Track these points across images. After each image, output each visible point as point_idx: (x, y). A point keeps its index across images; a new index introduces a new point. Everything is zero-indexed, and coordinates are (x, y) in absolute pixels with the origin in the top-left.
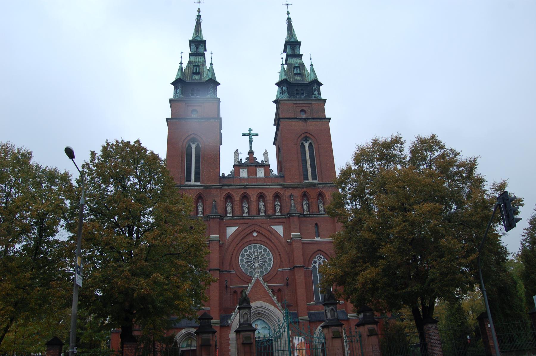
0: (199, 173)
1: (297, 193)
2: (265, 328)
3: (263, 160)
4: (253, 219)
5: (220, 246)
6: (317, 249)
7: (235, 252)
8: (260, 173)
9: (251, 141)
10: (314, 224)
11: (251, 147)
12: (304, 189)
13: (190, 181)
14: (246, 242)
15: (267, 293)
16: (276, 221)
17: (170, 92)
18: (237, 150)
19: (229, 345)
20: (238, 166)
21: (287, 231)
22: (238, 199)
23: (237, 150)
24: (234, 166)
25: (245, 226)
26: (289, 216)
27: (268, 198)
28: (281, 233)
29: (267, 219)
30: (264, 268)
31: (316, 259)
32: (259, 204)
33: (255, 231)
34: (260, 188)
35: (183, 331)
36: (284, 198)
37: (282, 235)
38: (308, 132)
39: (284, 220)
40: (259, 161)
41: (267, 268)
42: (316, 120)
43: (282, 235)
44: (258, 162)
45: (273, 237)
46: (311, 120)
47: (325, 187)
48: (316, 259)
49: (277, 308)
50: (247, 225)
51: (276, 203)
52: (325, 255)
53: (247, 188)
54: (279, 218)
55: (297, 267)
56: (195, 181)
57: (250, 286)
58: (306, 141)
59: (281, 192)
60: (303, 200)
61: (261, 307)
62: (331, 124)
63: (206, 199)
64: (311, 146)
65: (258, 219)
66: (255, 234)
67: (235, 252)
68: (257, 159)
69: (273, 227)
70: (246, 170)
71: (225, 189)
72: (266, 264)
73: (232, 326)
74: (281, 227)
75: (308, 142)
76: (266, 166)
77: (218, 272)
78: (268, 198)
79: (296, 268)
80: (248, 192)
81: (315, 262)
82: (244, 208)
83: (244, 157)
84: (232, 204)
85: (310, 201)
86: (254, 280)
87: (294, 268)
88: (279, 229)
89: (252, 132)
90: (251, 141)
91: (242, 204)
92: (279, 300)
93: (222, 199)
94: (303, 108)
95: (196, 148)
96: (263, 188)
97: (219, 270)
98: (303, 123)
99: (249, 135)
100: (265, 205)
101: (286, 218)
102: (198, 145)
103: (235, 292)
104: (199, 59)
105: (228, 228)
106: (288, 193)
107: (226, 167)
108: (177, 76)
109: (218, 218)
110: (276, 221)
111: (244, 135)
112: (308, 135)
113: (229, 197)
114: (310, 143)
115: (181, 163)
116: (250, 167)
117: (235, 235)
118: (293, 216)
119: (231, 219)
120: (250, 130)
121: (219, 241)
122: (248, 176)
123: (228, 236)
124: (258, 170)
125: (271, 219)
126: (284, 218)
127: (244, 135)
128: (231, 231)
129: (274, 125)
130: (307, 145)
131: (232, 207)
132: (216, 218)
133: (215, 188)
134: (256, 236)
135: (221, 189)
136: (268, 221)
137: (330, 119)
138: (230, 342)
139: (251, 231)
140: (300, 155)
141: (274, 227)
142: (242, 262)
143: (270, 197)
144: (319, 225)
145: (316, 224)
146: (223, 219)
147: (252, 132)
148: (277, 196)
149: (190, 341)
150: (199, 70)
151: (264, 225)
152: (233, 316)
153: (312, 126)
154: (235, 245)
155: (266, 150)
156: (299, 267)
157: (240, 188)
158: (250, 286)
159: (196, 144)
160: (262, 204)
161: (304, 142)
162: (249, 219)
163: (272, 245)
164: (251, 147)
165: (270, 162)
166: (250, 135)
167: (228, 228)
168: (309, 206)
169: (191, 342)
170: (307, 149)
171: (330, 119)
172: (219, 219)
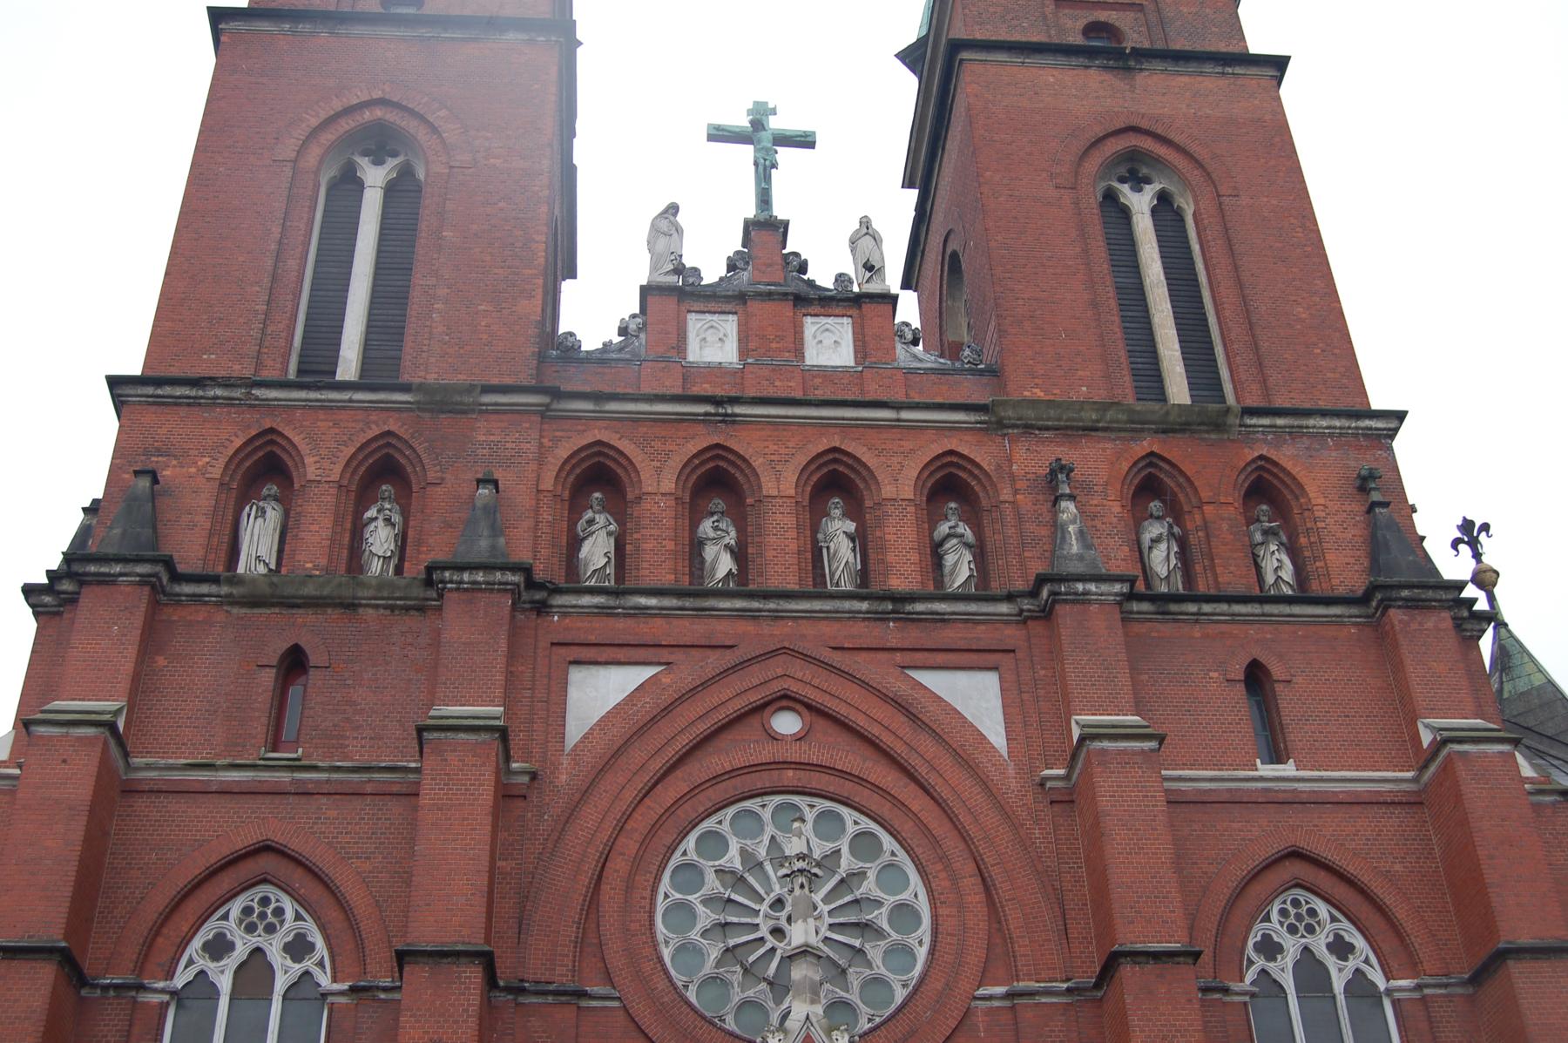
0: (399, 334)
1: (1101, 463)
3: (850, 270)
4: (777, 616)
5: (506, 795)
7: (628, 844)
9: (764, 171)
10: (1238, 670)
11: (764, 199)
14: (716, 779)
16: (948, 636)
18: (673, 209)
20: (672, 295)
22: (668, 484)
23: (673, 209)
24: (645, 291)
25: (715, 662)
26: (1045, 598)
27: (888, 491)
28: (995, 732)
29: (882, 617)
30: (856, 976)
31: (1275, 927)
33: (786, 701)
34: (825, 425)
36: (1006, 494)
37: (996, 735)
38: (1144, 124)
39: (1012, 635)
40: (822, 275)
41: (878, 981)
42: (1192, 67)
43: (996, 735)
44: (811, 283)
46: (1159, 65)
47: (1295, 434)
48: (1275, 927)
50: (730, 658)
54: (970, 620)
58: (1138, 182)
59: (983, 453)
60: (1139, 518)
62: (1290, 91)
63: (432, 475)
65: (810, 616)
66: (787, 723)
68: (803, 268)
69: (933, 680)
70: (729, 325)
71: (575, 418)
72: (875, 952)
75: (1150, 191)
77: (473, 975)
78: (888, 491)
79: (1127, 970)
80: (740, 442)
82: (710, 552)
83: (710, 252)
84: (621, 522)
85: (1194, 521)
87: (1112, 963)
88: (975, 698)
89: (775, 123)
90: (764, 171)
91: (694, 524)
93: (548, 483)
94: (1102, 16)
95: (390, 190)
96: (847, 427)
97: (487, 960)
98: (1108, 77)
100: (860, 539)
101: (1023, 619)
102: (406, 172)
105: (577, 675)
106: (1030, 458)
107: (596, 307)
109: (504, 588)
110: (948, 636)
111: (719, 135)
112: (1147, 144)
113: (599, 477)
114: (1163, 198)
115: (278, 259)
116: (754, 306)
117: (631, 725)
118: (1083, 599)
119: (603, 612)
121: (503, 733)
122: (743, 352)
123: (576, 726)
125: (904, 616)
126: (1004, 620)
127: (719, 135)
128: (598, 693)
129: (908, 183)
130: (1140, 203)
132: (490, 587)
133: (498, 410)
134: (799, 738)
135: (544, 414)
136: (892, 633)
137: (1279, 64)
139: (755, 698)
140: (1102, 266)
142: (682, 929)
143: (897, 479)
144: (1276, 670)
145: (1256, 678)
146: (542, 608)
147: (775, 123)
148: (949, 485)
153: (1161, 97)
154: (630, 795)
155: (865, 223)
156: (1156, 956)
157: (682, 419)
159: (391, 163)
160: (838, 530)
161: (1125, 188)
162: (742, 614)
163: (918, 802)
164: (764, 199)
166: (764, 139)
168: (1184, 554)
170: (1144, 225)
171: (1279, 64)
172: (515, 591)
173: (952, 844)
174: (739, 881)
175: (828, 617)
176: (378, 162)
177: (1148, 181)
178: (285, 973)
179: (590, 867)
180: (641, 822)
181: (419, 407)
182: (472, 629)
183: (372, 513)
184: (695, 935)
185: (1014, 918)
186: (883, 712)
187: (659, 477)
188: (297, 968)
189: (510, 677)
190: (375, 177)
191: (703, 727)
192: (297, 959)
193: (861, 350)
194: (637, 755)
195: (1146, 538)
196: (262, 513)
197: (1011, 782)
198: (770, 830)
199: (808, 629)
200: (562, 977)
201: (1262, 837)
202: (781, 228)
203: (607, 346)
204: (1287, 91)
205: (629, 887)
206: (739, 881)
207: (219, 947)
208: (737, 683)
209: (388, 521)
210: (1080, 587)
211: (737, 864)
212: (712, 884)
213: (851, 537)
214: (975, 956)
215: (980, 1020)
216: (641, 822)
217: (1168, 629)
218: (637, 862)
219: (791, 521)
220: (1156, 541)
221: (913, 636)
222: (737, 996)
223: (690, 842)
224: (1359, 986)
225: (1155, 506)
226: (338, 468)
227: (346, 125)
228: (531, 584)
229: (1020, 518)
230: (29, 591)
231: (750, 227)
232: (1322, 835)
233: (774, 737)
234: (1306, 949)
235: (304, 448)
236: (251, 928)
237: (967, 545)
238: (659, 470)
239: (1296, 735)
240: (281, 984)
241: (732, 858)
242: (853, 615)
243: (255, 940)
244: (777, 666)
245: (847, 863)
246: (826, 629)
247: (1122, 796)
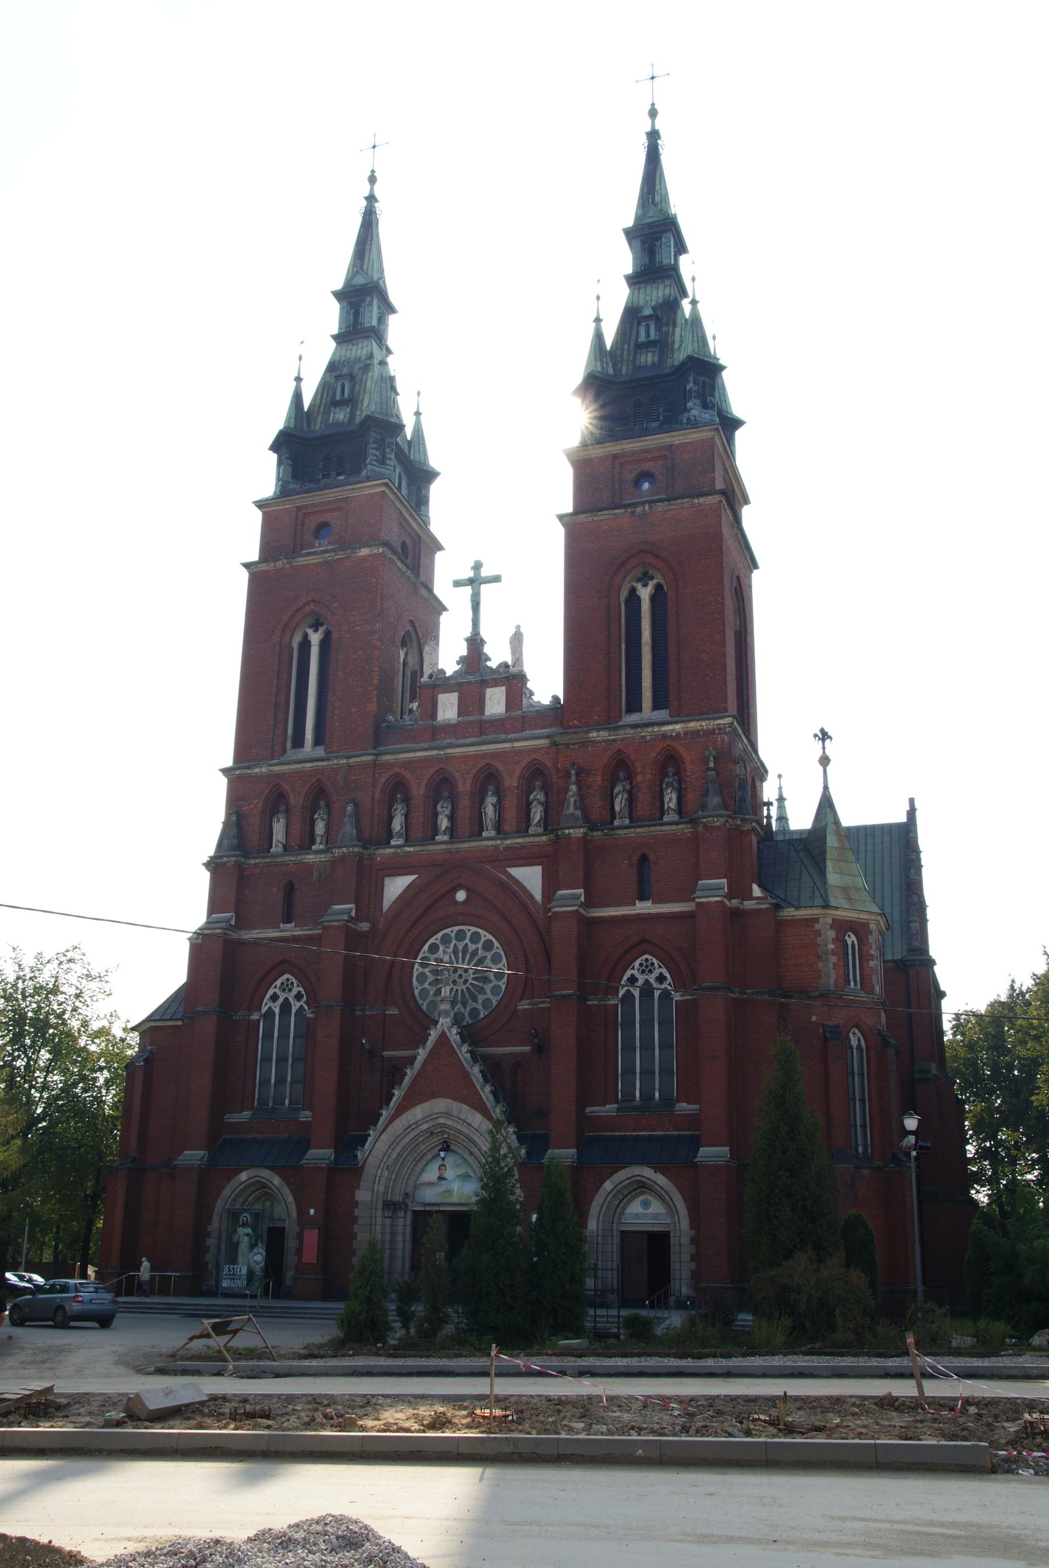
8: (495, 702)
13: (639, 709)
15: (466, 1077)
17: (264, 476)
19: (354, 1220)
21: (550, 885)
22: (422, 791)
32: (391, 806)
51: (532, 797)
56: (656, 707)
57: (422, 1054)
61: (448, 1114)
64: (325, 644)
73: (367, 1166)
74: (538, 869)
76: (513, 680)
78: (507, 783)
82: (440, 817)
84: (408, 806)
86: (434, 1034)
89: (485, 573)
91: (529, 793)
95: (653, 598)
99: (471, 582)
104: (658, 293)
108: (587, 366)
114: (658, 587)
120: (477, 566)
122: (459, 714)
123: (387, 904)
124: (489, 692)
131: (406, 816)
134: (465, 902)
138: (357, 1212)
141: (516, 872)
144: (652, 857)
147: (485, 573)
149: (268, 1204)
150: (352, 389)
152: (370, 1139)
155: (518, 627)
158: (422, 1054)
159: (321, 630)
160: (491, 800)
165: (529, 668)
167: (387, 881)
174: (464, 952)
177: (652, 578)
178: (295, 1006)
183: (316, 816)
184: (426, 985)
188: (298, 1004)
192: (299, 1001)
195: (615, 791)
196: (278, 821)
198: (454, 942)
202: (482, 642)
207: (274, 998)
209: (322, 819)
210: (567, 831)
211: (470, 950)
213: (494, 806)
220: (619, 793)
224: (665, 995)
226: (301, 799)
230: (204, 864)
234: (647, 980)
235: (289, 791)
236: (643, 972)
237: (541, 803)
238: (419, 784)
240: (657, 993)
243: (285, 995)
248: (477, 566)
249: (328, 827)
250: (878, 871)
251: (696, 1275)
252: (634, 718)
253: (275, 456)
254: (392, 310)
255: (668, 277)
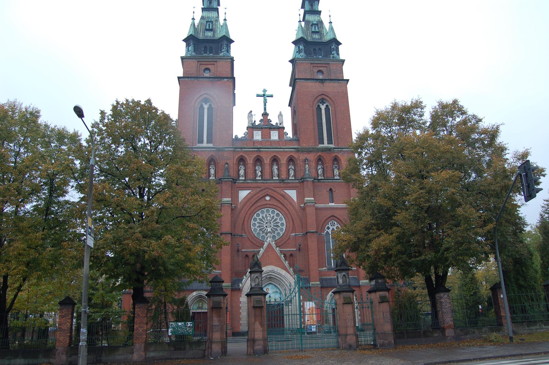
2: (276, 292)
3: (278, 122)
4: (266, 183)
5: (232, 210)
6: (330, 215)
7: (248, 216)
8: (274, 136)
10: (328, 189)
11: (265, 109)
12: (319, 154)
16: (290, 185)
18: (251, 112)
19: (240, 308)
20: (252, 127)
21: (301, 196)
22: (251, 162)
23: (251, 112)
24: (248, 128)
27: (282, 162)
29: (281, 183)
30: (276, 232)
32: (272, 167)
33: (268, 195)
34: (273, 152)
35: (194, 293)
36: (299, 162)
37: (295, 200)
39: (298, 185)
40: (274, 123)
42: (333, 81)
43: (295, 200)
45: (286, 201)
46: (328, 81)
47: (341, 151)
49: (289, 272)
52: (338, 221)
53: (260, 151)
54: (293, 183)
55: (309, 232)
57: (262, 251)
58: (323, 103)
59: (296, 156)
60: (317, 164)
61: (273, 271)
64: (327, 108)
65: (271, 183)
66: (268, 198)
67: (248, 216)
72: (278, 229)
75: (325, 105)
77: (230, 236)
78: (282, 162)
79: (308, 234)
81: (328, 228)
82: (257, 172)
83: (258, 119)
87: (307, 233)
88: (293, 194)
91: (255, 167)
92: (291, 265)
95: (208, 109)
96: (276, 152)
97: (231, 234)
100: (278, 169)
101: (300, 183)
102: (210, 105)
103: (247, 256)
105: (240, 192)
106: (302, 157)
110: (290, 185)
111: (258, 96)
112: (325, 97)
114: (327, 106)
116: (264, 130)
117: (248, 199)
118: (307, 181)
120: (265, 91)
122: (262, 138)
123: (240, 200)
125: (284, 183)
126: (297, 183)
127: (258, 96)
128: (243, 194)
129: (290, 86)
130: (323, 107)
131: (245, 170)
134: (269, 200)
135: (234, 151)
136: (282, 185)
138: (241, 305)
139: (264, 195)
141: (287, 192)
142: (255, 226)
144: (333, 190)
145: (331, 190)
146: (235, 183)
147: (267, 93)
148: (291, 160)
149: (201, 303)
150: (212, 26)
151: (278, 190)
152: (244, 280)
155: (280, 112)
157: (253, 151)
159: (208, 104)
160: (275, 167)
163: (284, 209)
164: (265, 109)
165: (285, 125)
166: (265, 96)
167: (240, 192)
168: (323, 171)
169: (202, 304)
170: (323, 112)
171: (348, 80)
173: (289, 215)
174: (261, 220)
175: (273, 183)
176: (206, 104)
177: (325, 103)
179: (243, 219)
180: (249, 213)
181: (216, 151)
182: (226, 187)
185: (296, 225)
186: (280, 197)
187: (250, 161)
189: (232, 193)
190: (206, 107)
191: (257, 199)
193: (279, 137)
194: (248, 204)
197: (297, 206)
199: (271, 185)
200: (240, 234)
201: (329, 214)
203: (242, 137)
204: (348, 86)
205: (248, 221)
206: (261, 220)
208: (261, 193)
212: (258, 220)
214: (291, 229)
215: (291, 238)
216: (249, 213)
217: (319, 184)
218: (248, 219)
219: (268, 167)
221: (285, 185)
222: (261, 235)
223: (255, 215)
225: (320, 163)
227: (201, 98)
228: (233, 179)
229: (300, 167)
231: (263, 115)
232: (337, 214)
233: (266, 200)
239: (335, 199)
241: (261, 217)
242: (277, 182)
244: (266, 190)
245: (275, 217)
246: (273, 184)
247: (310, 211)
248: (265, 91)
249: (215, 171)
250: (283, 279)
251: (361, 321)
252: (321, 146)
253: (185, 43)
254: (340, 44)
255: (318, 14)
